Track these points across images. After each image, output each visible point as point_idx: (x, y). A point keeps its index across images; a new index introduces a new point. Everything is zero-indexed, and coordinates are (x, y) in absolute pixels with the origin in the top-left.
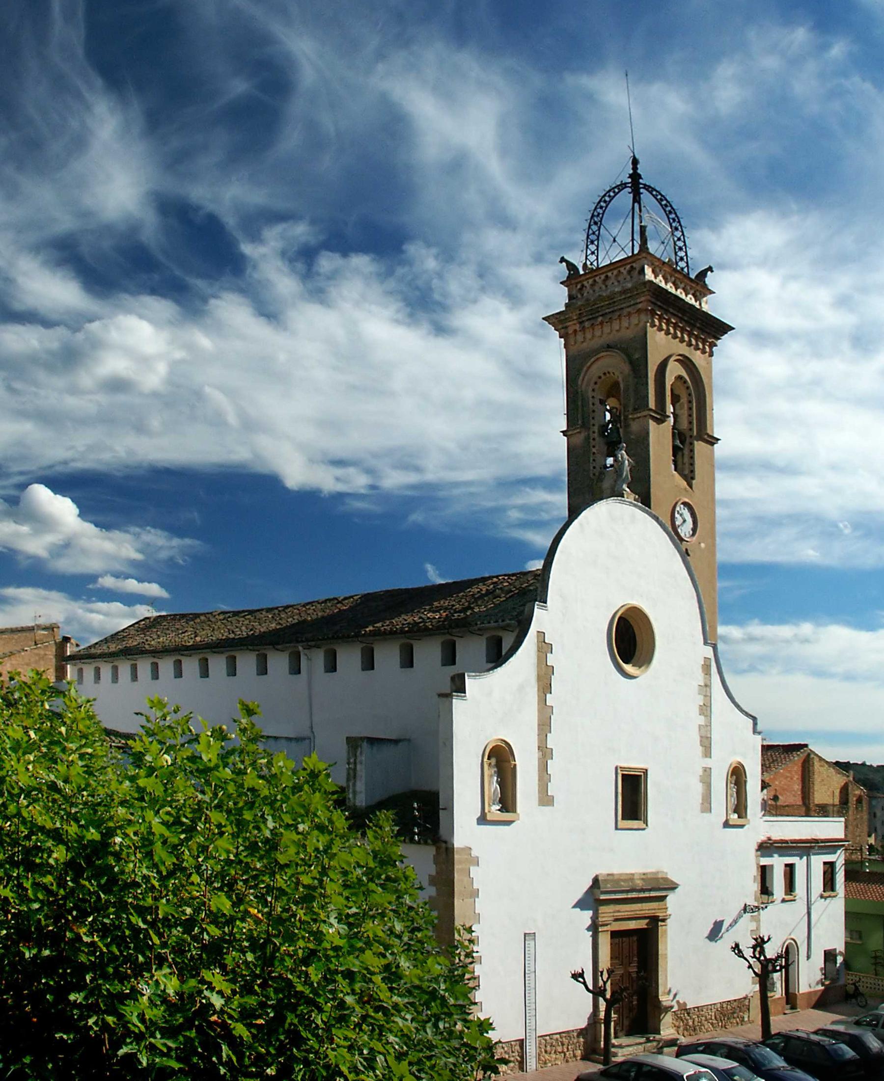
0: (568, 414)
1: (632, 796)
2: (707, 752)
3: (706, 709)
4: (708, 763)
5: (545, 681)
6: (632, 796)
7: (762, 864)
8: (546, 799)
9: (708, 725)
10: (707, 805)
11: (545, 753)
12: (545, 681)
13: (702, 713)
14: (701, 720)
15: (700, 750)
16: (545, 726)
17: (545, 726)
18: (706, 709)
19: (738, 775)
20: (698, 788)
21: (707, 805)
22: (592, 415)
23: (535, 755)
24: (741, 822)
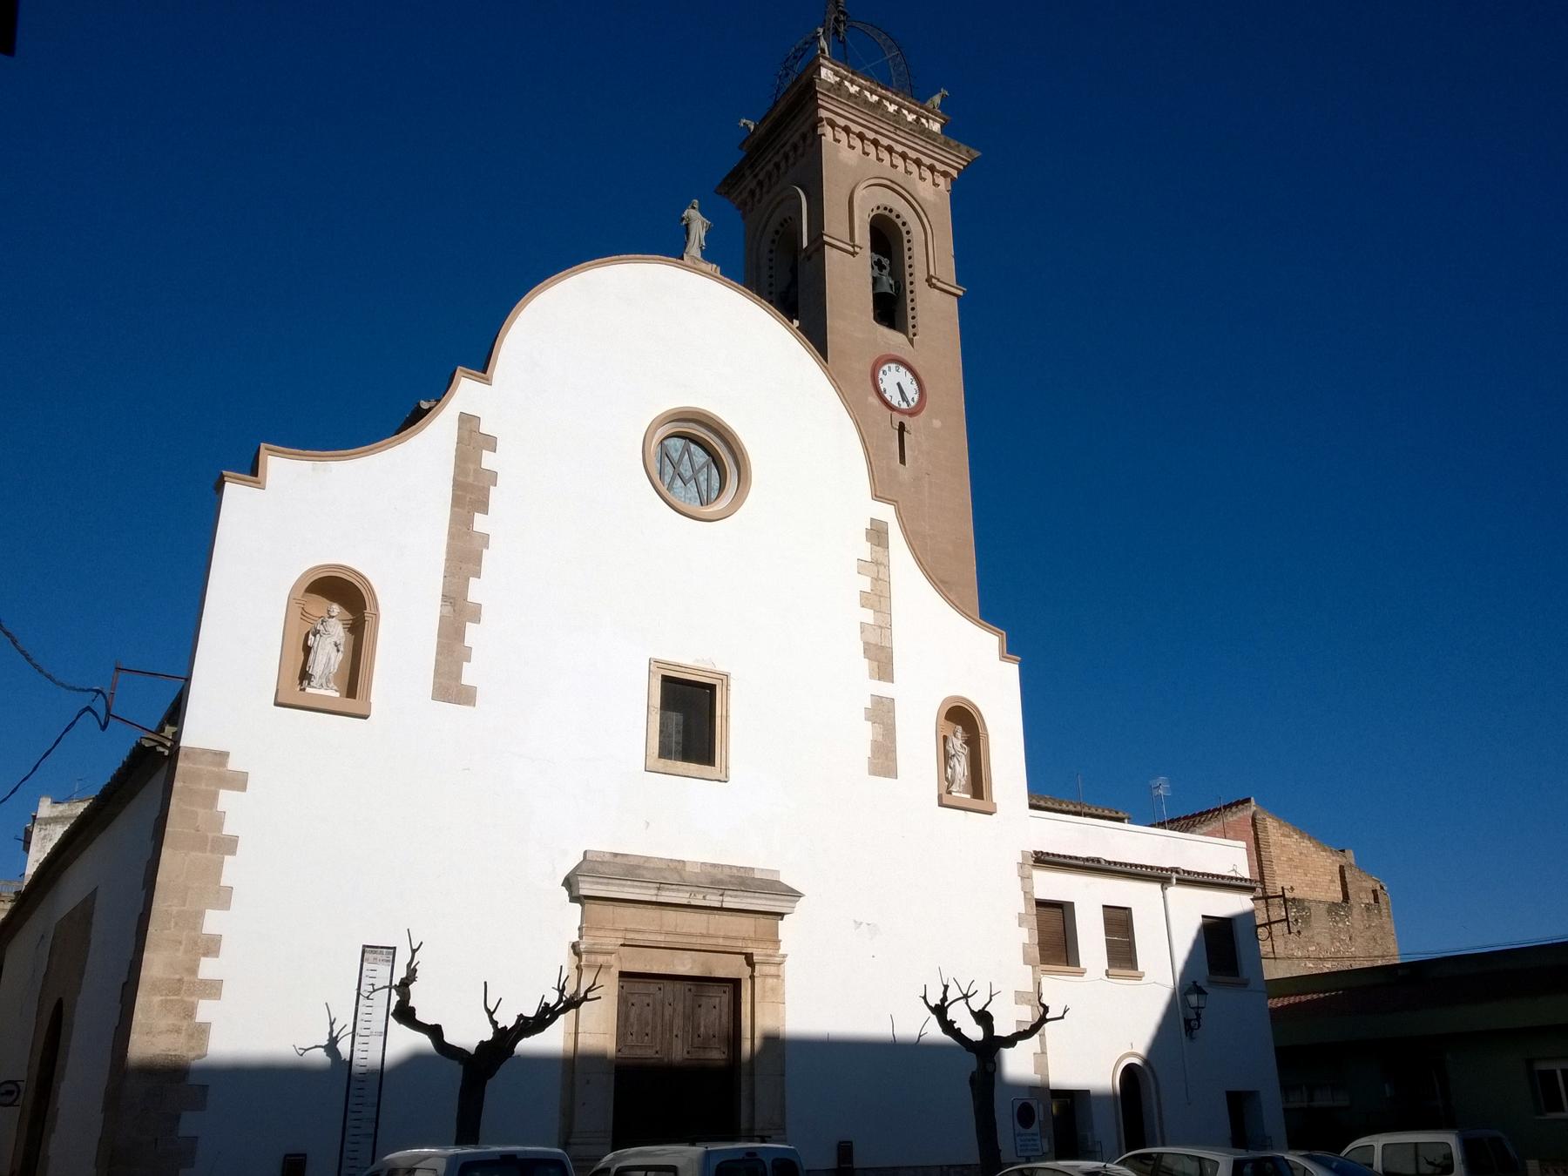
0: (955, 257)
1: (690, 718)
2: (881, 661)
3: (878, 598)
4: (884, 689)
5: (471, 492)
6: (690, 718)
7: (1042, 894)
8: (451, 687)
9: (885, 627)
10: (884, 760)
11: (457, 613)
12: (471, 492)
13: (866, 600)
14: (868, 616)
15: (864, 665)
16: (464, 556)
17: (464, 556)
18: (878, 598)
19: (962, 719)
20: (865, 733)
21: (884, 760)
22: (904, 230)
23: (431, 611)
24: (1053, 885)
